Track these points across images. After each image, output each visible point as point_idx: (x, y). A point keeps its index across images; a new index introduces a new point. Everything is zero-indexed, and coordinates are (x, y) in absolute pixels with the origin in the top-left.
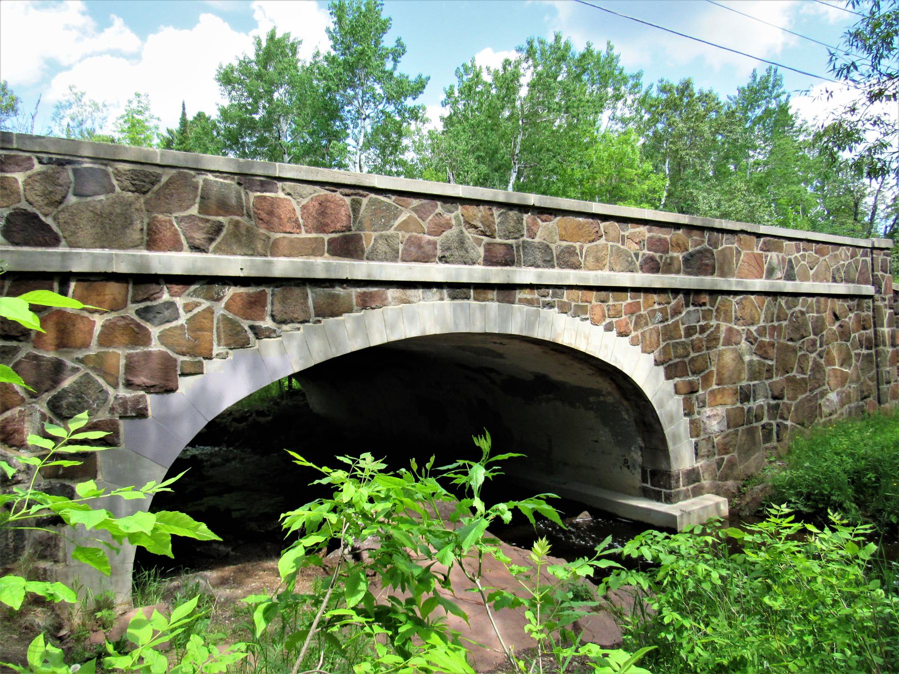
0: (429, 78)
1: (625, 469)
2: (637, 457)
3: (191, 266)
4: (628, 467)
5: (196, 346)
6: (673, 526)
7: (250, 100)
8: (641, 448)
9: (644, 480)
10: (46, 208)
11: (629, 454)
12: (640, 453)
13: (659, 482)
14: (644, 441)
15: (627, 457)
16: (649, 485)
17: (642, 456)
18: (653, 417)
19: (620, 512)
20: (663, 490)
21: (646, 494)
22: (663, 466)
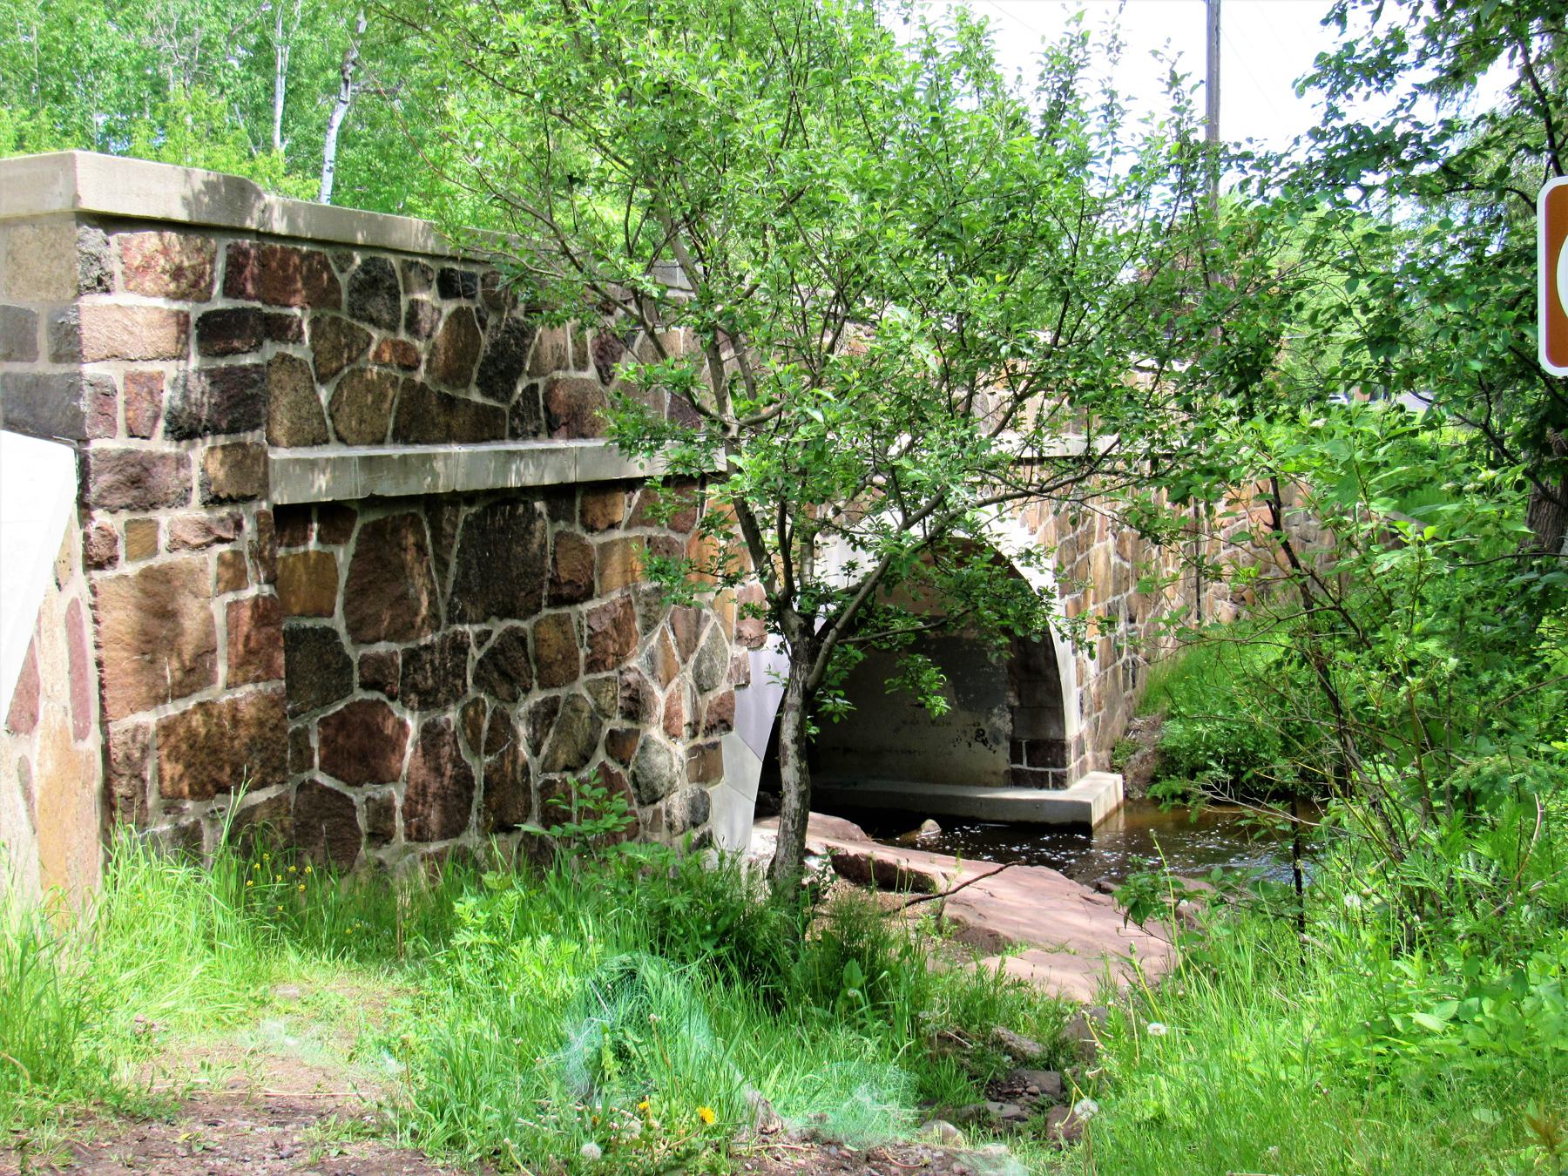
0: (1325, 22)
1: (978, 746)
2: (1003, 723)
3: (610, 502)
4: (985, 742)
5: (255, 978)
6: (1083, 819)
7: (1420, 265)
8: (1012, 709)
9: (1015, 757)
10: (274, 154)
11: (988, 719)
12: (1008, 717)
13: (1044, 757)
14: (1019, 696)
15: (983, 726)
16: (1024, 766)
17: (1012, 720)
18: (1047, 658)
19: (983, 814)
20: (1051, 770)
21: (1018, 780)
22: (1052, 733)
